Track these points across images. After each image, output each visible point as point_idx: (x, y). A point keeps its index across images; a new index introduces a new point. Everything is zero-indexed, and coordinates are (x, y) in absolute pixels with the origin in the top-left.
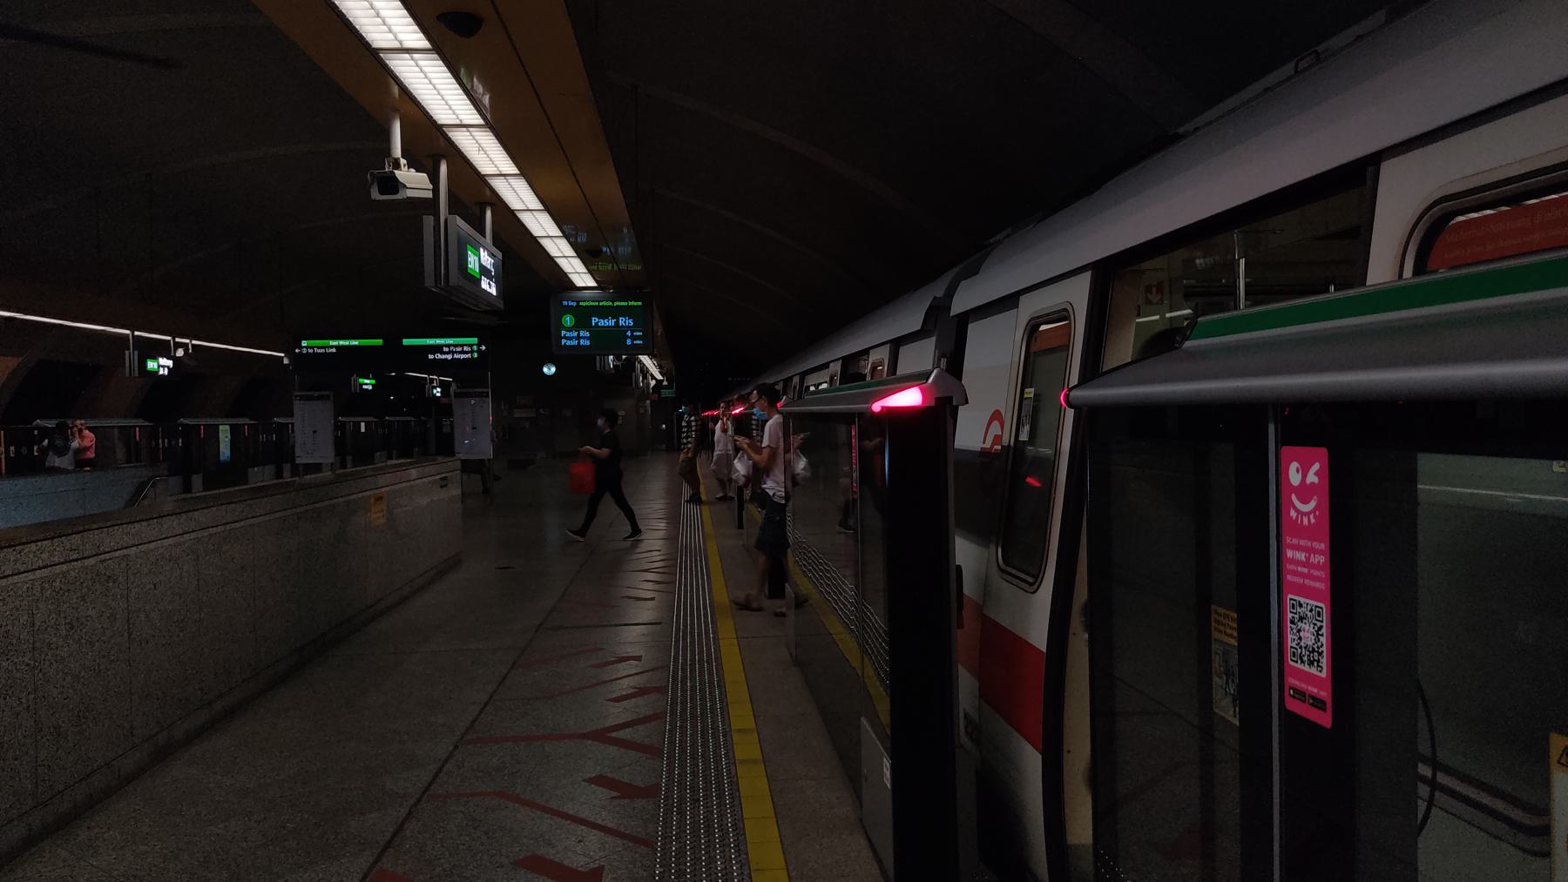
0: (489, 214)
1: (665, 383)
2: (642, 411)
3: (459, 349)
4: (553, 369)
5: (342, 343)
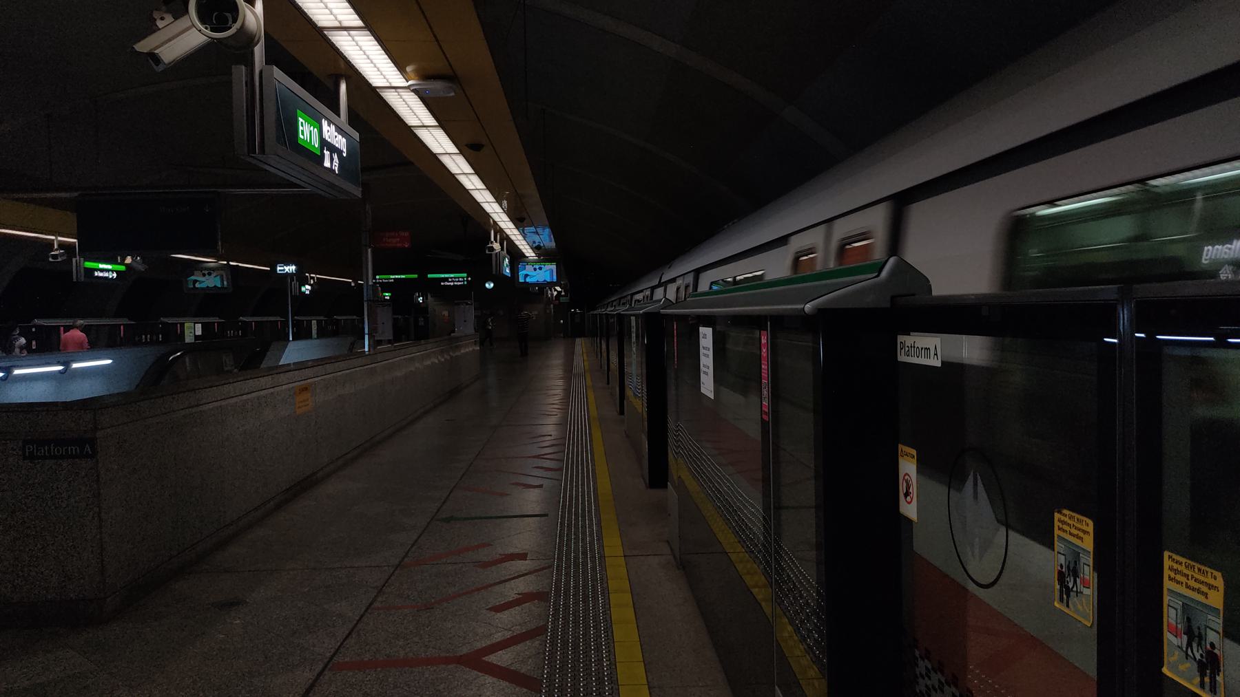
0: (343, 87)
1: (563, 293)
2: (548, 311)
3: (457, 280)
4: (492, 285)
5: (397, 277)
